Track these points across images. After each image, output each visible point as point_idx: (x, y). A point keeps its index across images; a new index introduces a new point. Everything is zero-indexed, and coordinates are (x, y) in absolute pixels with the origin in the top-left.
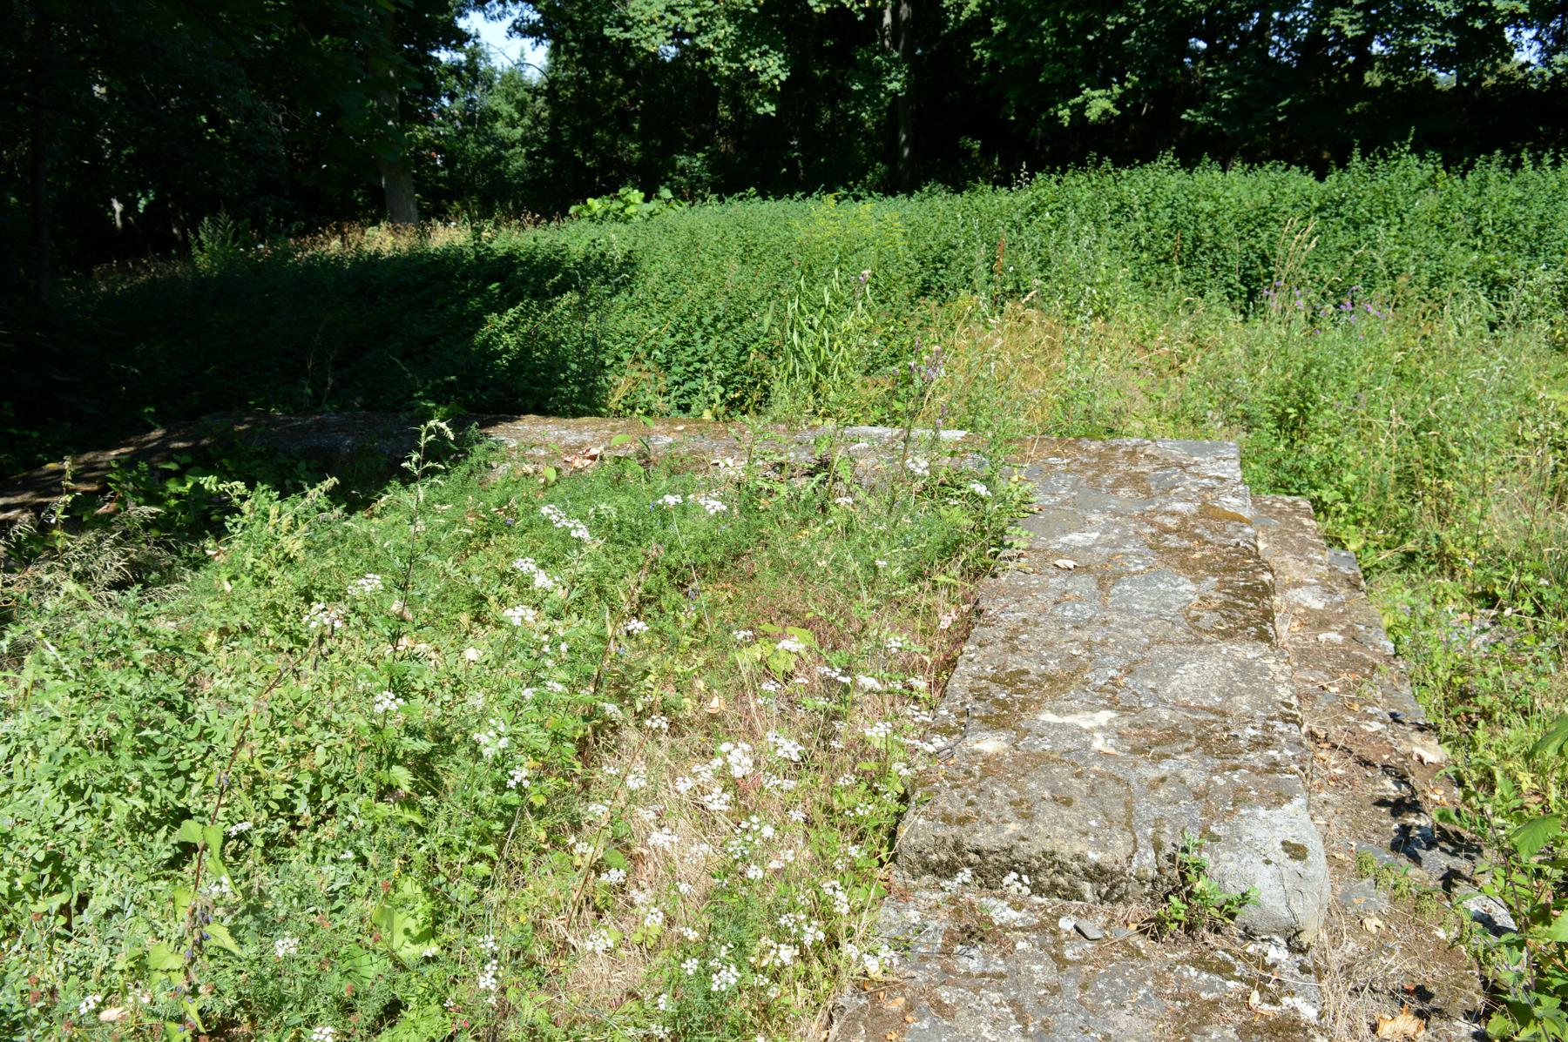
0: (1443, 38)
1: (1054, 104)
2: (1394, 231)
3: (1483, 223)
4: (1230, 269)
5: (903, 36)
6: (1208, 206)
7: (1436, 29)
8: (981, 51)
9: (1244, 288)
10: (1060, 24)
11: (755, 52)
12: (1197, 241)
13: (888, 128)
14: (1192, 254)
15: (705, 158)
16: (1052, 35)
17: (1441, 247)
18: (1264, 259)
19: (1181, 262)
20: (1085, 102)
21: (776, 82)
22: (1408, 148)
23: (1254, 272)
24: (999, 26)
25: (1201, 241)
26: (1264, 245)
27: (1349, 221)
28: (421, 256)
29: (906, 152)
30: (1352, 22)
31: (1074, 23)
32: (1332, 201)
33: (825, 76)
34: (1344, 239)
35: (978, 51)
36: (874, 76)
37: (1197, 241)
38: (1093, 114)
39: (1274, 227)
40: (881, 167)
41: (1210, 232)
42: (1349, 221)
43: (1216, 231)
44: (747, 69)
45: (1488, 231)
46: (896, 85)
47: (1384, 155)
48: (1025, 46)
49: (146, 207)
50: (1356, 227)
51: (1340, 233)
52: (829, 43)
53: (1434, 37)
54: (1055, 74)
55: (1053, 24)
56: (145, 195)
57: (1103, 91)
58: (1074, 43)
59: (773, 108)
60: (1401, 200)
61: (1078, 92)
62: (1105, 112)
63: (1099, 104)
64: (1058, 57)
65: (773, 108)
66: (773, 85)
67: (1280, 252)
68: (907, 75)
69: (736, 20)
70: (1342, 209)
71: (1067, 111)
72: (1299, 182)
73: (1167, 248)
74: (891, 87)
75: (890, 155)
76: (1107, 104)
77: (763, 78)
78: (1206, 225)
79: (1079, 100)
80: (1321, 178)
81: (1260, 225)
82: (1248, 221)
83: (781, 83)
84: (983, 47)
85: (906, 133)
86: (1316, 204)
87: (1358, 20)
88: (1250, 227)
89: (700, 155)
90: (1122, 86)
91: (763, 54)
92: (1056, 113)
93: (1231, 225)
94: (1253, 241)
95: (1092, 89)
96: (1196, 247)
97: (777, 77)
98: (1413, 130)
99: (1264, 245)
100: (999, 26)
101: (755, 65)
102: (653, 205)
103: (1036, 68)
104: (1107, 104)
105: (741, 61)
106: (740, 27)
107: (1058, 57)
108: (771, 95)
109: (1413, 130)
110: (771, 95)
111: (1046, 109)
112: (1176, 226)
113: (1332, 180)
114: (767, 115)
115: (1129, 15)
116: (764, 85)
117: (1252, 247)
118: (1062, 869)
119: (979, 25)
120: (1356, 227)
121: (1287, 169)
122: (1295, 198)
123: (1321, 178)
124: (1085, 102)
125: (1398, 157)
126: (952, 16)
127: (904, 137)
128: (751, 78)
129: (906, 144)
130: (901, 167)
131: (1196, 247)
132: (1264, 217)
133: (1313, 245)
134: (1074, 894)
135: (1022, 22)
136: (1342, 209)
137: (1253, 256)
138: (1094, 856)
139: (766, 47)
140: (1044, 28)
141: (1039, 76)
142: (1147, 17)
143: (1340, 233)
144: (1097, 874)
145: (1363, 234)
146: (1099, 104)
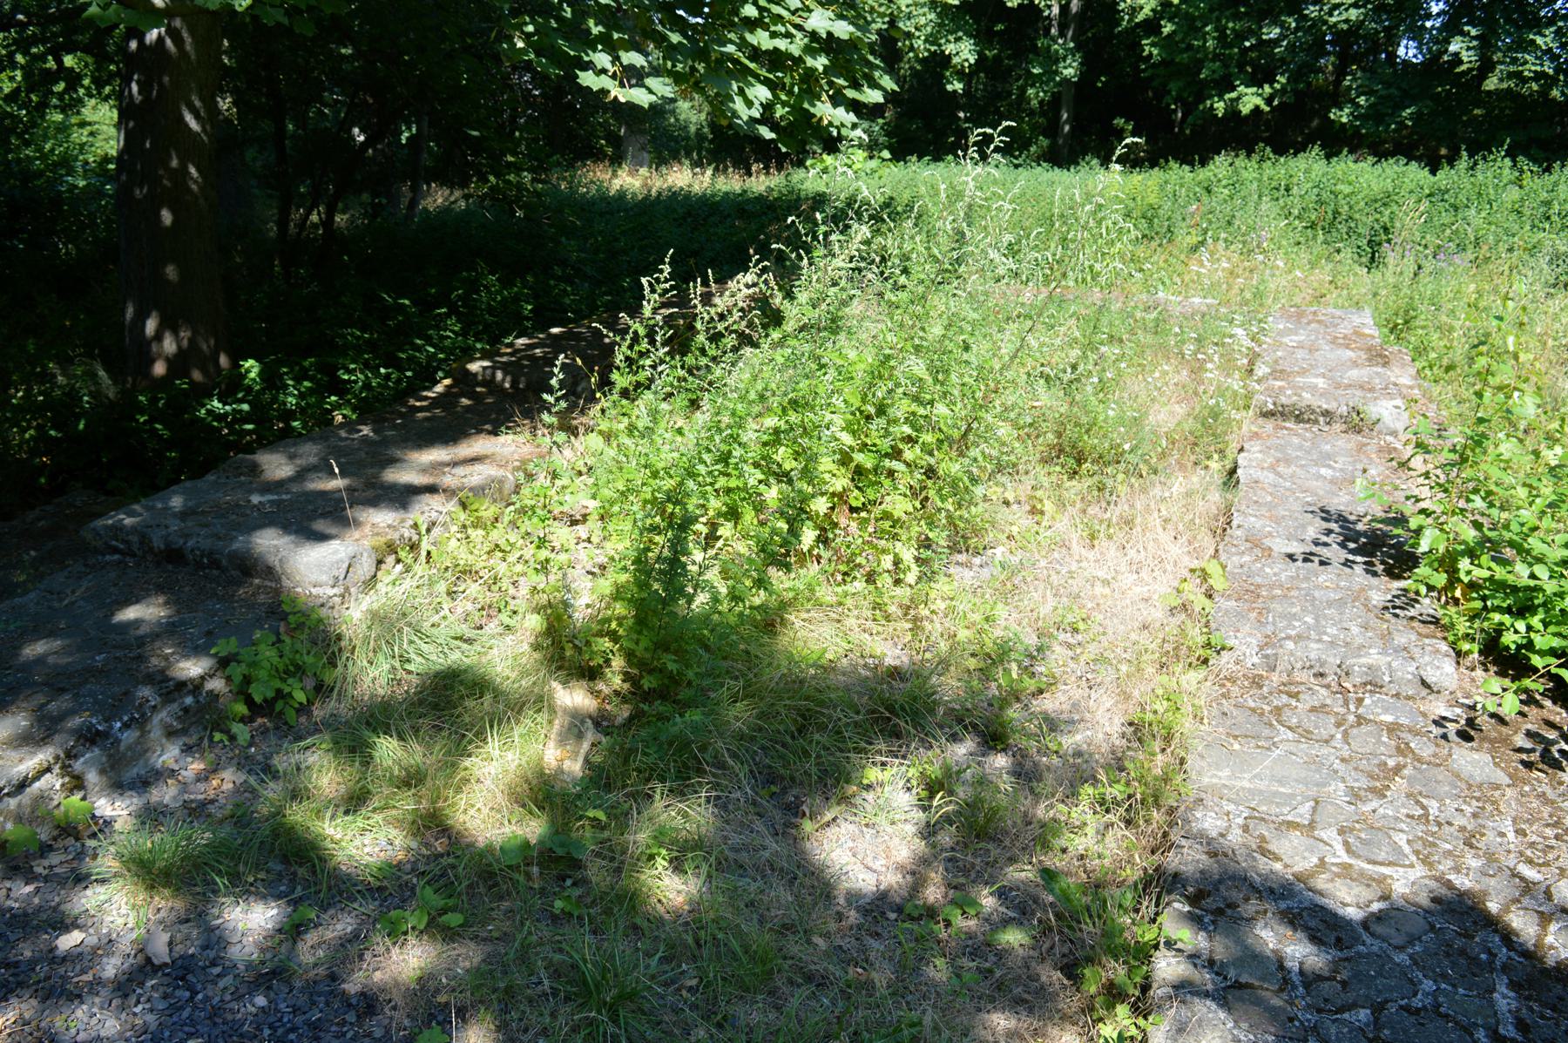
0: (1542, 65)
1: (1210, 97)
2: (1483, 214)
3: (1551, 211)
4: (1359, 235)
5: (1073, 26)
6: (1347, 189)
7: (1536, 58)
8: (1149, 48)
9: (1369, 250)
10: (1221, 30)
11: (951, 38)
12: (1336, 213)
13: (1054, 104)
14: (1332, 224)
15: (885, 124)
16: (1214, 38)
17: (1517, 227)
18: (1386, 229)
19: (1323, 229)
20: (1239, 98)
21: (966, 64)
22: (1503, 153)
23: (1377, 239)
24: (1168, 28)
25: (1339, 213)
26: (1386, 219)
27: (1452, 205)
28: (713, 196)
29: (1067, 128)
30: (1469, 49)
31: (1233, 30)
32: (1440, 190)
33: (994, 56)
34: (1446, 218)
35: (1147, 48)
36: (1052, 60)
37: (1336, 213)
38: (1245, 109)
39: (1395, 208)
40: (1044, 142)
41: (1346, 208)
42: (1452, 205)
43: (1351, 208)
44: (943, 52)
45: (1555, 218)
46: (1069, 72)
47: (1484, 158)
48: (1190, 47)
49: (408, 139)
50: (1456, 210)
51: (1444, 214)
52: (999, 27)
53: (1533, 64)
54: (1214, 72)
55: (1216, 29)
56: (409, 128)
57: (1255, 89)
58: (1231, 46)
59: (961, 86)
60: (1492, 191)
61: (1233, 89)
62: (1257, 108)
63: (1250, 99)
64: (1216, 57)
65: (961, 86)
66: (963, 66)
67: (1398, 225)
68: (1080, 64)
69: (935, 9)
70: (1446, 197)
71: (1222, 104)
72: (1415, 174)
73: (1313, 217)
74: (1066, 72)
75: (1052, 130)
76: (1259, 101)
77: (956, 60)
78: (1344, 202)
79: (1234, 95)
80: (1433, 172)
81: (1384, 204)
82: (1376, 201)
83: (970, 65)
84: (1153, 45)
85: (1068, 112)
86: (1427, 191)
87: (1473, 48)
88: (1377, 205)
89: (881, 121)
90: (1272, 88)
91: (958, 40)
92: (1212, 105)
93: (1362, 203)
94: (1378, 216)
95: (1247, 86)
96: (1335, 218)
97: (967, 60)
98: (1508, 141)
99: (1386, 219)
100: (1168, 28)
101: (950, 48)
102: (874, 163)
103: (1199, 64)
104: (1259, 101)
105: (940, 45)
106: (939, 15)
107: (1216, 57)
108: (960, 74)
109: (1508, 141)
110: (960, 74)
111: (1203, 101)
112: (1321, 202)
113: (1441, 174)
114: (955, 91)
115: (1282, 27)
116: (955, 66)
117: (1377, 220)
118: (1313, 412)
119: (1151, 26)
120: (1456, 210)
121: (1407, 164)
122: (1412, 186)
123: (1433, 172)
124: (1239, 98)
125: (1495, 160)
126: (1127, 17)
127: (1065, 116)
128: (946, 60)
129: (1066, 122)
130: (1061, 142)
131: (1335, 218)
132: (1387, 199)
133: (1422, 220)
134: (1316, 422)
135: (1191, 26)
136: (1446, 197)
137: (1377, 227)
138: (1325, 406)
139: (960, 34)
140: (1208, 33)
141: (1200, 73)
142: (1297, 29)
143: (1444, 214)
144: (1326, 413)
145: (1460, 216)
146: (1250, 99)
